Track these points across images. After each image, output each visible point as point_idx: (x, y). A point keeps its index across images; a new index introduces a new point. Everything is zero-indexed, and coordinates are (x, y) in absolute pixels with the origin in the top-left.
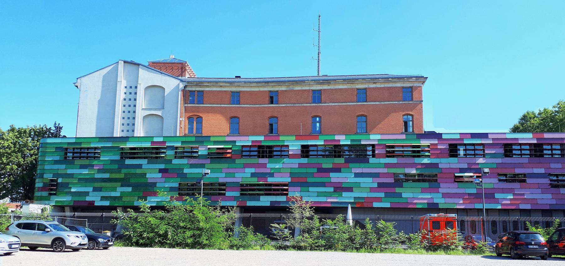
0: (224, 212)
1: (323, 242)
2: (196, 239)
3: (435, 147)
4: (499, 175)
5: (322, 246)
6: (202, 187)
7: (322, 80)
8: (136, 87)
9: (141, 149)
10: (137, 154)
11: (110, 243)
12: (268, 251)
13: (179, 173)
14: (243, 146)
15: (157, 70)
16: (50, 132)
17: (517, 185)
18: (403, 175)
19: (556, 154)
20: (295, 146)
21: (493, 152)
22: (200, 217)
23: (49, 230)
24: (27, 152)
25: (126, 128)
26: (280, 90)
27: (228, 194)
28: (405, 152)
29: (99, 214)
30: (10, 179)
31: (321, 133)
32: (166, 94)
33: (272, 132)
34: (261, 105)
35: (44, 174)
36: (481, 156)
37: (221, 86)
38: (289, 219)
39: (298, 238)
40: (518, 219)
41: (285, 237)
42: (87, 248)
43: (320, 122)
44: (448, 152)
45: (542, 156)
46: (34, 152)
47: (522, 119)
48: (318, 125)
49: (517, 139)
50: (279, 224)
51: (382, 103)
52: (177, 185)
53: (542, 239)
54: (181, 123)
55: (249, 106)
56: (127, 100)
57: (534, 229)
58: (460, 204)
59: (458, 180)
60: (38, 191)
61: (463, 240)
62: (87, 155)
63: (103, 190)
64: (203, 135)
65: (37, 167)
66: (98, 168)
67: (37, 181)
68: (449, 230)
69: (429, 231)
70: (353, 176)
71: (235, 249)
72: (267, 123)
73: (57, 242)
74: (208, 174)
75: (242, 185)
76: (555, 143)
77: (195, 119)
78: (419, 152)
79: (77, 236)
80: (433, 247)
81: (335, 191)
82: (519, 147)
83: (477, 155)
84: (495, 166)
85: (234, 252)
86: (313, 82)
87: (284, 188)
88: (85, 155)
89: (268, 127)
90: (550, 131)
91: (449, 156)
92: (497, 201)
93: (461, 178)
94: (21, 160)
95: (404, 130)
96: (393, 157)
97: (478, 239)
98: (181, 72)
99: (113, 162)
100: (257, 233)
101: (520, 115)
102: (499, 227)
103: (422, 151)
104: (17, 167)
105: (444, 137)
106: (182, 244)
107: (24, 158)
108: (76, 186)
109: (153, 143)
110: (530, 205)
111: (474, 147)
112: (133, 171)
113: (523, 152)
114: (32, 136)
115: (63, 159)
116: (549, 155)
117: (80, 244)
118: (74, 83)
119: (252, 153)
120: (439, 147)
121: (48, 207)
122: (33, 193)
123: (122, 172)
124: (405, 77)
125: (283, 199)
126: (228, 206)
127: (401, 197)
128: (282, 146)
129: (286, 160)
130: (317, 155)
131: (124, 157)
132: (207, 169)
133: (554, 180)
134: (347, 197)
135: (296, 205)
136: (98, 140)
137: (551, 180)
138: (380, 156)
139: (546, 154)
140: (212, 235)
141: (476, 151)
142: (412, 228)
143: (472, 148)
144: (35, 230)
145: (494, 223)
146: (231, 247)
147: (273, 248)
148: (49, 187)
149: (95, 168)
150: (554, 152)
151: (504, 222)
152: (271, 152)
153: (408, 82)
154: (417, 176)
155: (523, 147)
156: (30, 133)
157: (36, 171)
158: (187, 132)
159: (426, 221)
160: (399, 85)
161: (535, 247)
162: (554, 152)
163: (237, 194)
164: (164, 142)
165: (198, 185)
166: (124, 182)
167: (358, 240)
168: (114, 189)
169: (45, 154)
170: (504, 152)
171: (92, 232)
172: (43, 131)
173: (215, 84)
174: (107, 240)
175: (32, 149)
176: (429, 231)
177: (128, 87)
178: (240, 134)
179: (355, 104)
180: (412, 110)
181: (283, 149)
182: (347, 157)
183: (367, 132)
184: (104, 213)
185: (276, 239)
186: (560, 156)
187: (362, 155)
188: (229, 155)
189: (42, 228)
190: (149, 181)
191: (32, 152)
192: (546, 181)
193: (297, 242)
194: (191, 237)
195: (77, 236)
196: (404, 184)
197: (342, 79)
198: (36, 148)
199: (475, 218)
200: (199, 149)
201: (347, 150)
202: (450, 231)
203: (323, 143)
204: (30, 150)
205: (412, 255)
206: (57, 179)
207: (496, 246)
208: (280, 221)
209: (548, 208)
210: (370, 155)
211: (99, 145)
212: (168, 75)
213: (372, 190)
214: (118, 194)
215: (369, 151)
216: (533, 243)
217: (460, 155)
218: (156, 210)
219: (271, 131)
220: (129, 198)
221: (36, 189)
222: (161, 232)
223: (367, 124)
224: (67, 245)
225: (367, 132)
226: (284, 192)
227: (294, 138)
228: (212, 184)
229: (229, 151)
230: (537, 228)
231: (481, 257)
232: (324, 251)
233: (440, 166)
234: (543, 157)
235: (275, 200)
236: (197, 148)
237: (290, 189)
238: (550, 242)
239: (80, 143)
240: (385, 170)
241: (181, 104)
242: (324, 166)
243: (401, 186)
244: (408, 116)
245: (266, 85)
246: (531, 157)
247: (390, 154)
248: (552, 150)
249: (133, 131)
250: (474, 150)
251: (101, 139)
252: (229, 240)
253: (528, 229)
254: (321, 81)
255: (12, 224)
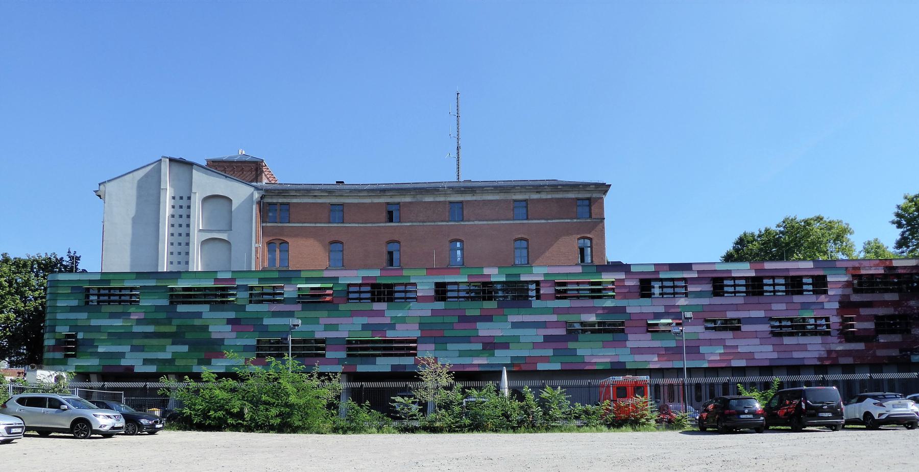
0: (323, 381)
1: (468, 422)
2: (284, 420)
3: (621, 284)
4: (706, 321)
5: (465, 426)
6: (290, 345)
7: (463, 187)
8: (189, 198)
9: (199, 289)
10: (195, 298)
11: (158, 426)
12: (388, 435)
13: (255, 323)
14: (349, 285)
15: (219, 172)
16: (62, 265)
17: (728, 335)
18: (579, 324)
19: (779, 291)
20: (425, 287)
21: (698, 289)
22: (290, 388)
23: (66, 407)
24: (30, 295)
25: (175, 258)
26: (403, 201)
27: (329, 355)
28: (580, 292)
29: (141, 385)
30: (5, 334)
31: (463, 265)
32: (234, 208)
33: (391, 264)
34: (374, 223)
35: (55, 326)
36: (681, 296)
37: (315, 196)
38: (417, 389)
39: (431, 416)
40: (728, 380)
41: (412, 416)
42: (124, 432)
43: (462, 249)
44: (639, 291)
45: (761, 293)
46: (40, 294)
47: (737, 243)
48: (459, 252)
49: (730, 271)
50: (403, 397)
51: (549, 221)
52: (255, 343)
53: (758, 406)
54: (257, 252)
55: (357, 225)
56: (177, 216)
57: (746, 394)
58: (654, 362)
59: (651, 329)
60: (49, 351)
61: (657, 411)
62: (120, 298)
63: (146, 349)
64: (290, 269)
65: (44, 317)
66: (136, 317)
67: (46, 336)
68: (638, 398)
69: (612, 401)
70: (510, 326)
71: (341, 432)
72: (384, 250)
73: (78, 425)
74: (298, 325)
75: (349, 342)
76: (778, 275)
77: (278, 245)
78: (599, 291)
79: (109, 417)
80: (617, 423)
81: (484, 349)
82: (732, 283)
83: (677, 293)
84: (700, 309)
85: (340, 437)
86: (451, 189)
87: (411, 345)
88: (117, 298)
89: (385, 257)
90: (773, 259)
91: (640, 297)
92: (702, 357)
93: (656, 327)
94: (21, 306)
95: (579, 259)
96: (565, 298)
97: (676, 409)
98: (255, 176)
99: (158, 308)
100: (372, 410)
101: (735, 237)
102: (705, 392)
103: (605, 289)
104: (15, 316)
105: (633, 269)
106: (264, 426)
107: (25, 302)
108: (104, 344)
109: (217, 280)
110: (745, 361)
111: (674, 284)
112: (189, 322)
113: (738, 289)
114: (35, 270)
115: (83, 304)
116: (770, 292)
117: (113, 428)
118: (96, 192)
119: (363, 296)
120: (627, 283)
121: (64, 375)
122: (42, 353)
123: (173, 323)
124: (580, 185)
125: (409, 361)
126: (328, 373)
127: (576, 355)
128: (406, 285)
129: (413, 304)
130: (458, 297)
131: (176, 302)
132: (298, 318)
133: (777, 326)
134: (502, 357)
135: (427, 370)
136: (134, 276)
137: (773, 327)
138: (548, 297)
139: (767, 291)
140: (307, 414)
141: (675, 289)
142: (592, 396)
143: (671, 284)
144: (45, 407)
145: (698, 386)
146: (335, 430)
147: (395, 430)
148: (65, 345)
149: (132, 317)
150: (777, 288)
151: (712, 385)
152: (391, 293)
153: (584, 192)
154: (596, 325)
155: (737, 282)
156: (32, 265)
157: (44, 321)
158: (266, 265)
159: (608, 387)
160: (572, 195)
161: (748, 416)
162: (777, 288)
163: (343, 354)
164: (233, 280)
165: (284, 342)
166: (176, 338)
167: (515, 417)
168: (162, 349)
169: (55, 297)
170: (712, 289)
171: (131, 410)
172: (51, 262)
173: (306, 193)
174: (153, 421)
175: (37, 290)
176: (612, 401)
177: (177, 198)
178: (344, 267)
179: (512, 222)
180: (589, 233)
181: (409, 288)
182: (501, 299)
183: (529, 264)
184: (148, 383)
185: (400, 418)
186: (784, 294)
187: (521, 296)
188: (328, 298)
189: (55, 404)
190: (214, 336)
191: (37, 294)
192: (766, 328)
193: (429, 422)
194: (277, 416)
195: (109, 417)
196: (581, 336)
197: (492, 186)
198: (43, 288)
199: (674, 381)
200: (285, 289)
201: (500, 290)
202: (639, 399)
203: (466, 280)
204: (33, 291)
205: (588, 434)
206: (76, 334)
207: (700, 418)
208: (404, 392)
209: (767, 363)
210: (532, 297)
211: (138, 284)
212: (230, 178)
213: (536, 345)
214: (169, 356)
215: (532, 290)
216: (746, 411)
217: (654, 294)
218: (224, 378)
219: (391, 262)
220: (185, 360)
221: (46, 349)
222: (235, 410)
223: (528, 252)
224: (94, 428)
225: (528, 263)
226: (411, 352)
227: (424, 272)
228: (305, 341)
229: (328, 292)
230: (752, 391)
231: (680, 433)
232: (468, 434)
233: (628, 310)
234: (763, 295)
235: (398, 364)
236: (282, 288)
237: (420, 347)
238: (768, 410)
239: (108, 281)
240: (554, 318)
241: (256, 222)
242: (469, 313)
243: (576, 340)
244: (585, 240)
245: (382, 194)
246: (747, 295)
247: (561, 294)
248: (774, 285)
249: (187, 263)
250: (674, 287)
251: (140, 275)
252: (331, 420)
253: (740, 394)
254: (463, 189)
255: (11, 398)
